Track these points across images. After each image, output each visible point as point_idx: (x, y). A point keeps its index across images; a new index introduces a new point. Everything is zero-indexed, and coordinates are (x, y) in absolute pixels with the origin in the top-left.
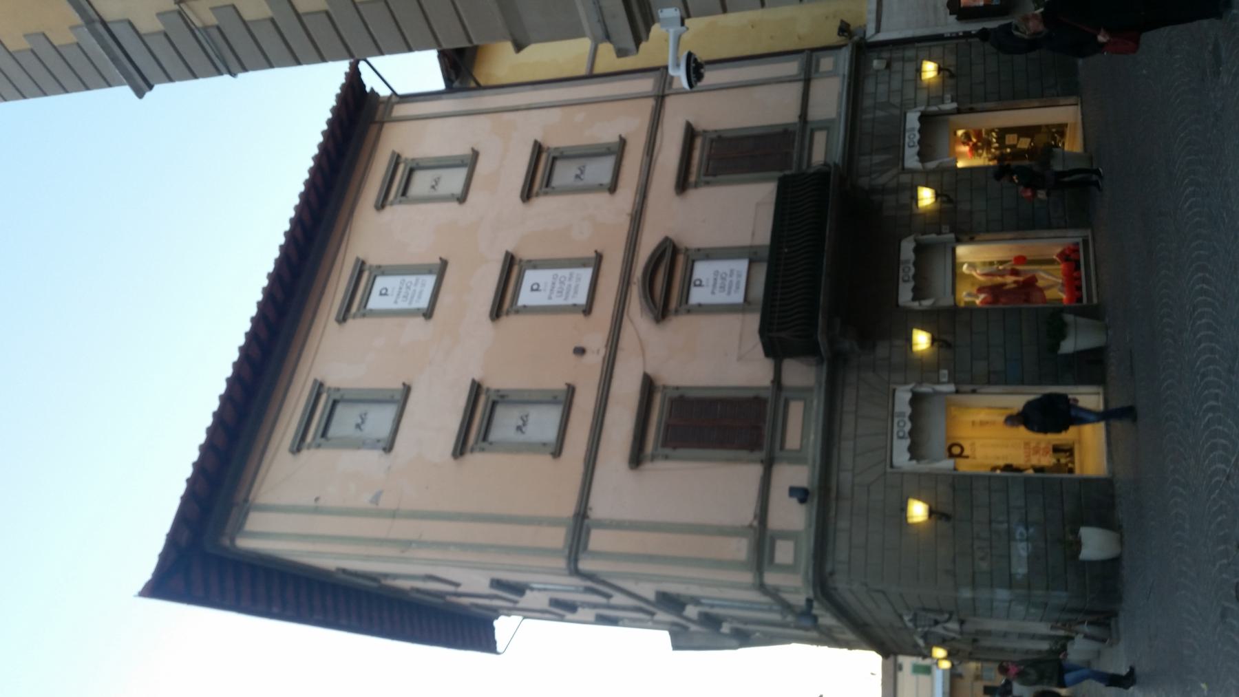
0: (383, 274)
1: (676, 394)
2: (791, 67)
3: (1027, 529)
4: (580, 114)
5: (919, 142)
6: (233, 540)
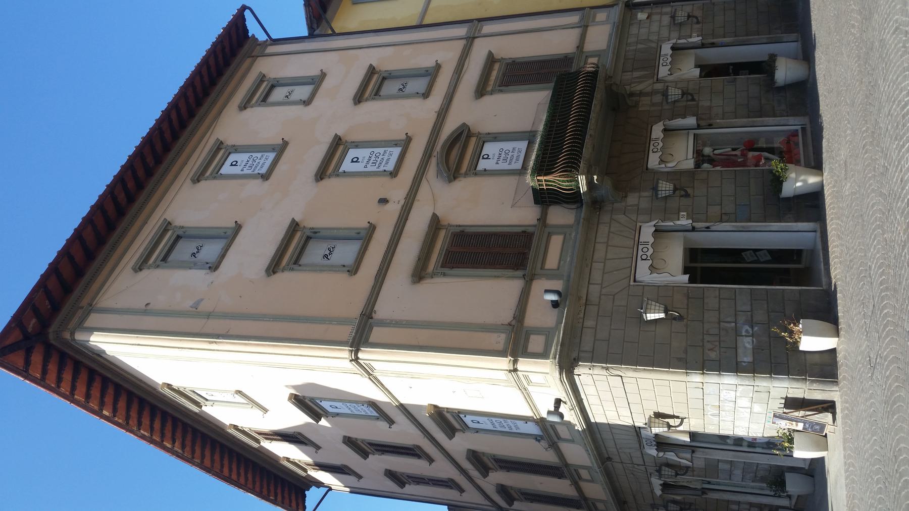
0: (357, 147)
1: (458, 230)
2: (574, 19)
3: (752, 328)
4: (407, 51)
6: (72, 334)
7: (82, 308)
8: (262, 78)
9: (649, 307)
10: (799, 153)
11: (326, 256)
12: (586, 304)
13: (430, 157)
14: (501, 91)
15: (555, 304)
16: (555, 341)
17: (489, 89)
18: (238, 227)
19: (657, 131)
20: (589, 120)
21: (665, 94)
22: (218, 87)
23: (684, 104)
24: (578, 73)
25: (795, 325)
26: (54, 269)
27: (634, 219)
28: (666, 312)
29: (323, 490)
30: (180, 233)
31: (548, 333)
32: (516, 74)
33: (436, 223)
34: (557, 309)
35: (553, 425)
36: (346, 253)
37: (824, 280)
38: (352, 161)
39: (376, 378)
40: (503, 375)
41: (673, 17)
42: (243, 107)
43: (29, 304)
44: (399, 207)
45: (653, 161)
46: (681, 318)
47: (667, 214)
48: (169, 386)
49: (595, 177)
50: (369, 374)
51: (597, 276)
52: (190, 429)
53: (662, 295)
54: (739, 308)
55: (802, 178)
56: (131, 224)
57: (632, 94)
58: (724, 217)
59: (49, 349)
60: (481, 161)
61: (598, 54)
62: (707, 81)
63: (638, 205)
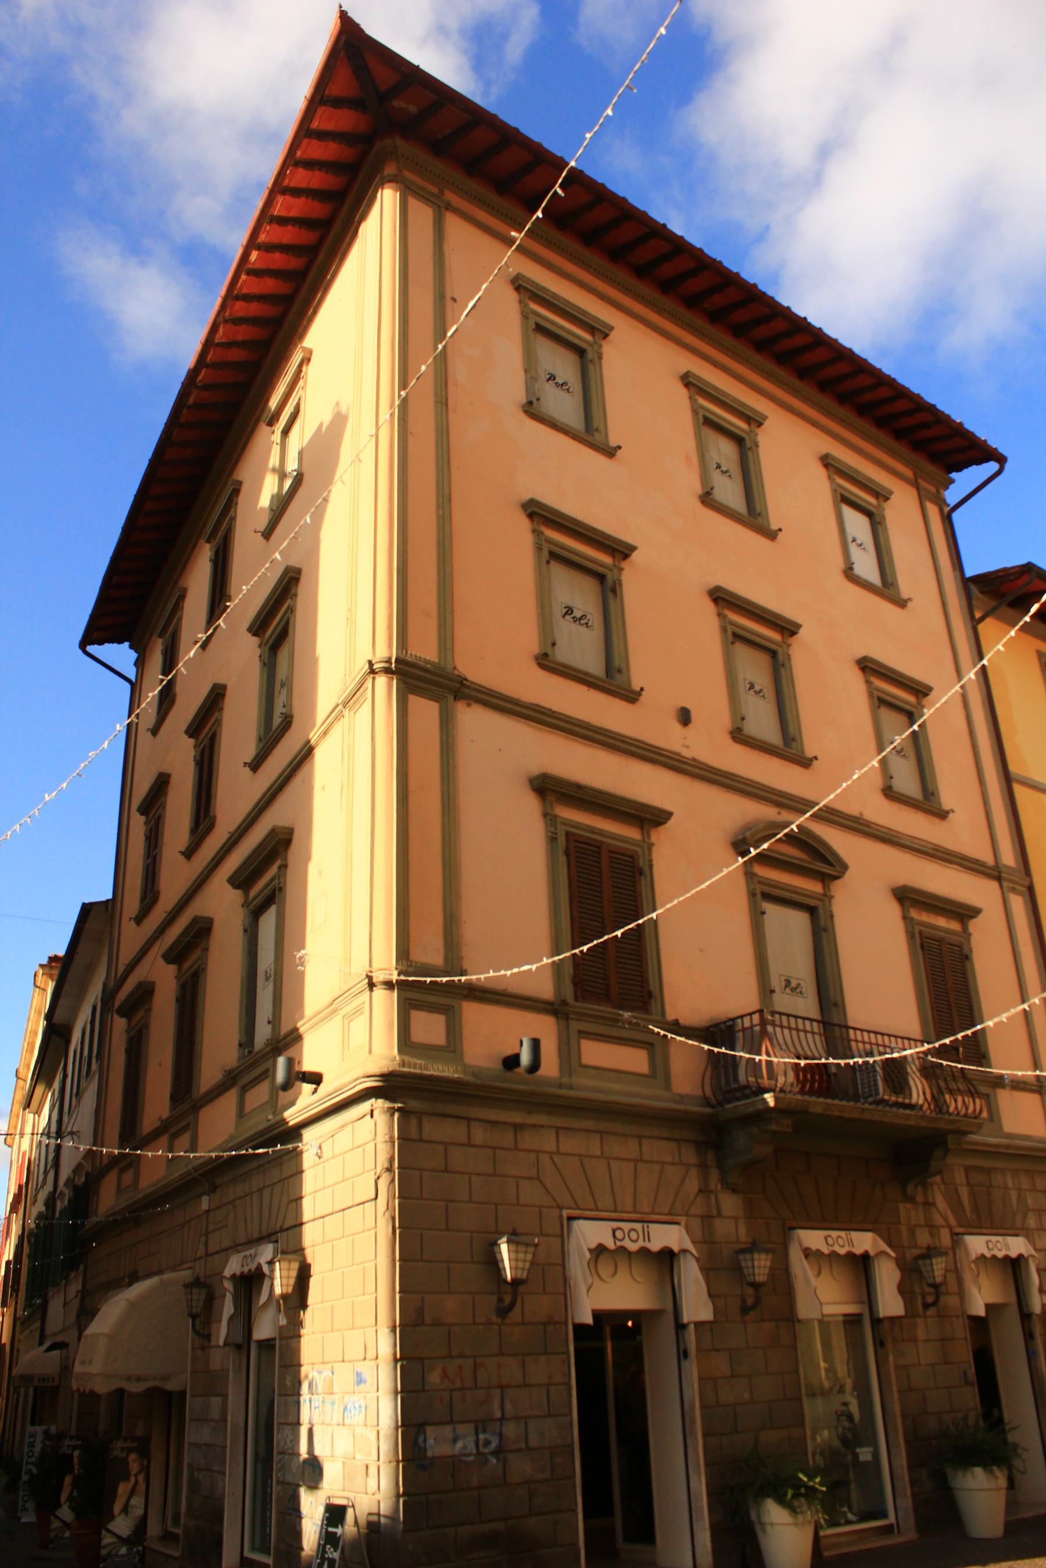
3: (493, 1453)
5: (994, 1257)
8: (882, 495)
9: (522, 1248)
11: (569, 611)
17: (914, 914)
18: (610, 452)
19: (864, 1242)
23: (917, 1289)
27: (693, 1210)
28: (516, 1282)
30: (590, 355)
31: (453, 1046)
33: (650, 818)
34: (500, 1066)
35: (269, 1073)
36: (582, 648)
39: (341, 716)
40: (360, 967)
42: (827, 462)
48: (306, 360)
50: (345, 704)
51: (570, 1144)
62: (960, 1330)
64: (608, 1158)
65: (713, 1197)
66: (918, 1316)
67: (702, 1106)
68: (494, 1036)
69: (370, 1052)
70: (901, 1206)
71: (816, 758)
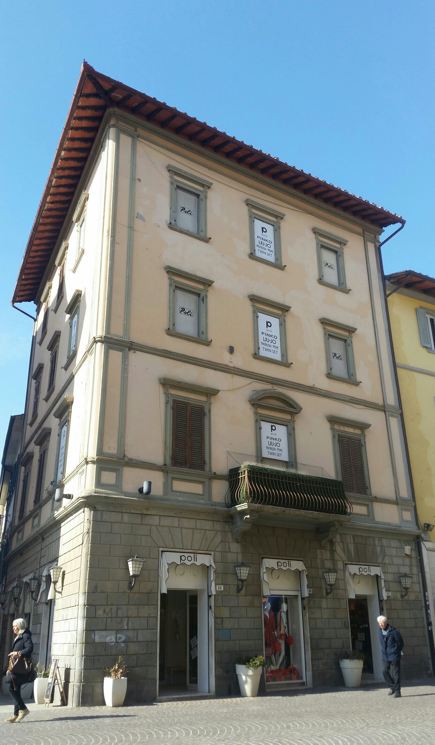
0: (281, 324)
1: (206, 411)
2: (404, 493)
4: (372, 358)
6: (114, 126)
7: (136, 131)
9: (138, 563)
10: (280, 680)
11: (183, 310)
12: (142, 514)
13: (272, 383)
14: (334, 437)
15: (141, 490)
16: (109, 492)
17: (336, 427)
18: (207, 240)
19: (297, 565)
20: (302, 510)
21: (334, 570)
22: (334, 209)
23: (324, 586)
24: (344, 498)
25: (122, 673)
26: (161, 107)
28: (134, 576)
29: (34, 314)
31: (117, 486)
32: (351, 448)
33: (211, 393)
34: (138, 492)
36: (186, 324)
37: (164, 698)
38: (267, 322)
41: (405, 575)
43: (131, 93)
44: (227, 363)
45: (269, 563)
46: (131, 588)
47: (222, 576)
48: (87, 199)
49: (248, 516)
50: (88, 351)
51: (166, 522)
52: (65, 213)
53: (150, 573)
54: (139, 632)
55: (249, 680)
56: (209, 158)
57: (332, 543)
58: (219, 621)
59: (103, 108)
60: (270, 424)
61: (371, 514)
62: (345, 605)
63: (230, 552)
64: (181, 528)
65: (227, 544)
66: (323, 598)
67: (224, 507)
68: (136, 480)
69: (85, 488)
70: (318, 551)
71: (292, 363)
